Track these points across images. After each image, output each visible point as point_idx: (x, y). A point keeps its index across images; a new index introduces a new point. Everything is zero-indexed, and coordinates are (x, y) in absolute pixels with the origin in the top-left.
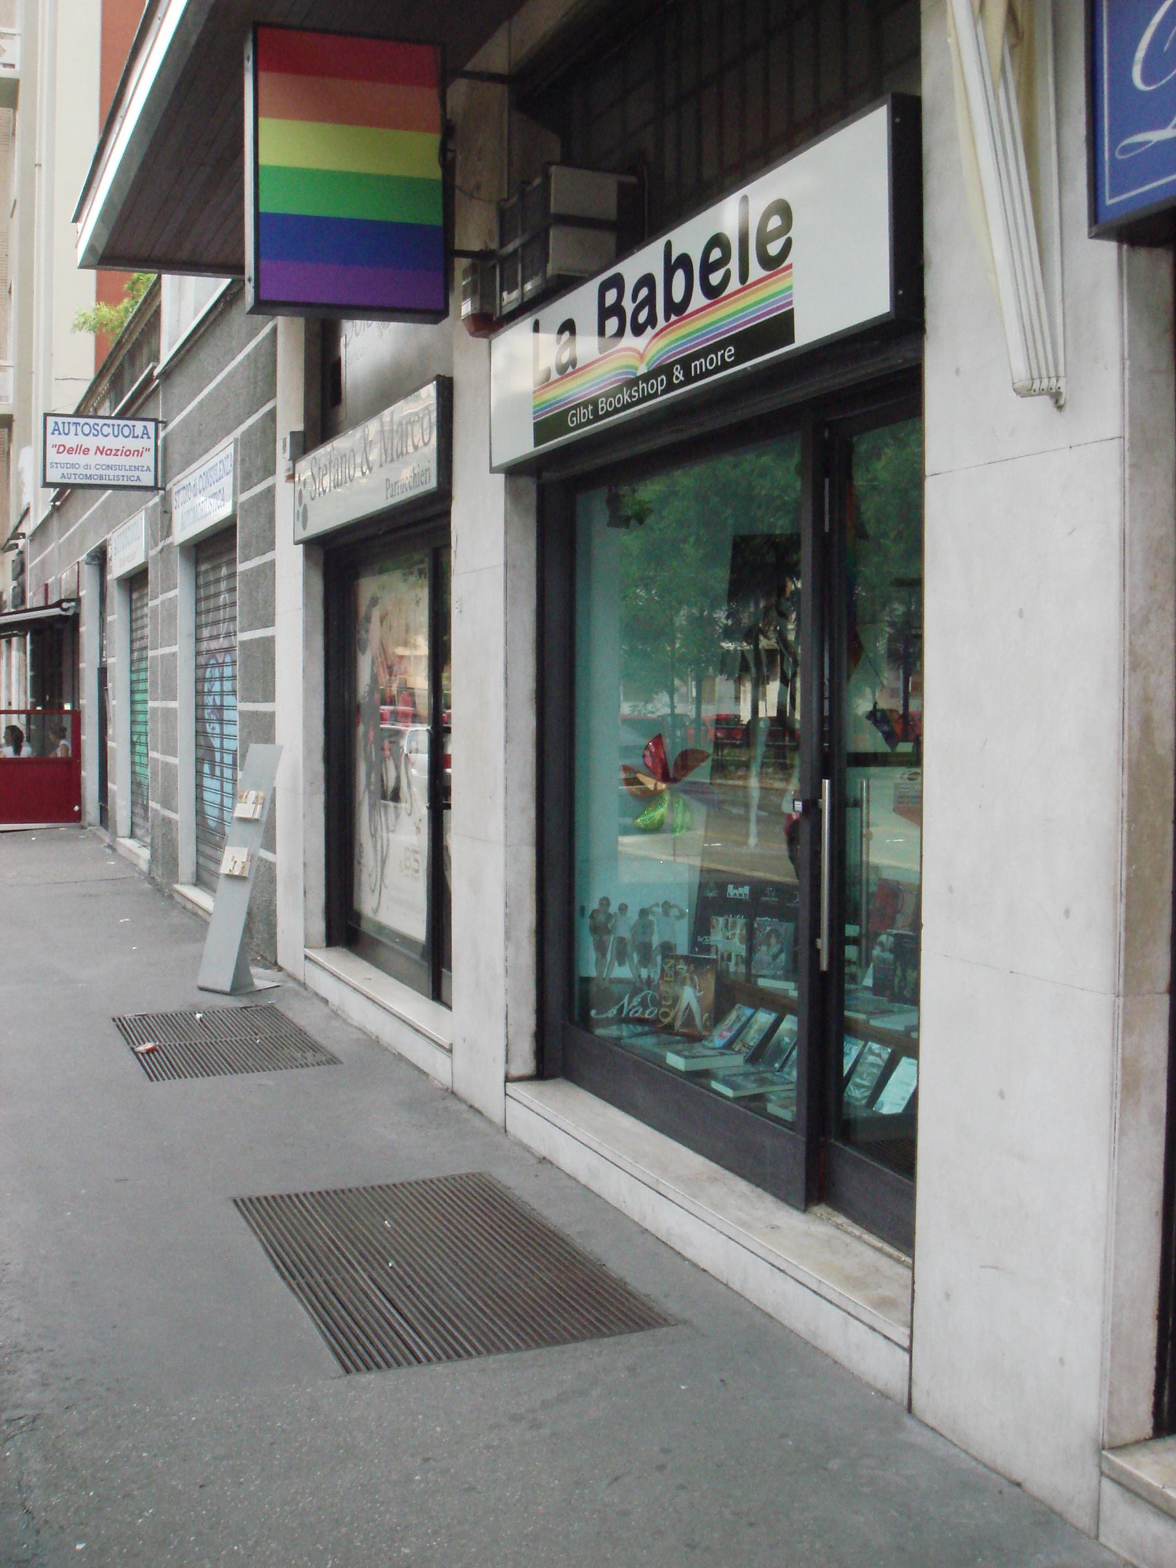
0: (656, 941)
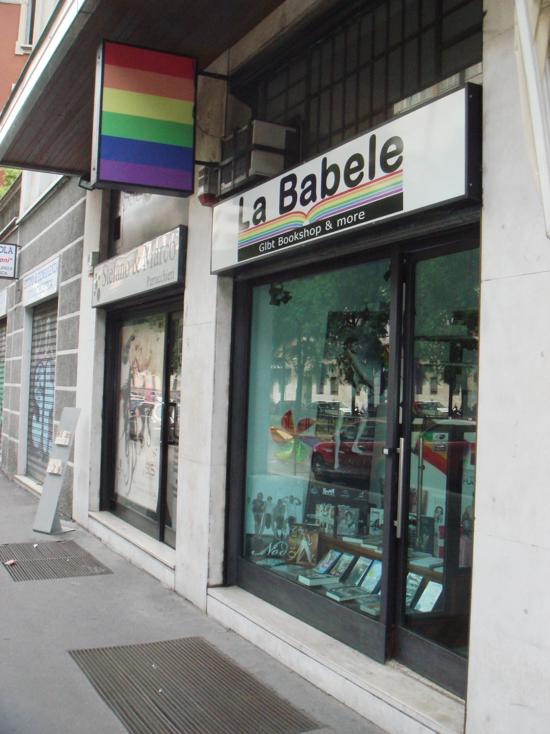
0: (286, 516)
